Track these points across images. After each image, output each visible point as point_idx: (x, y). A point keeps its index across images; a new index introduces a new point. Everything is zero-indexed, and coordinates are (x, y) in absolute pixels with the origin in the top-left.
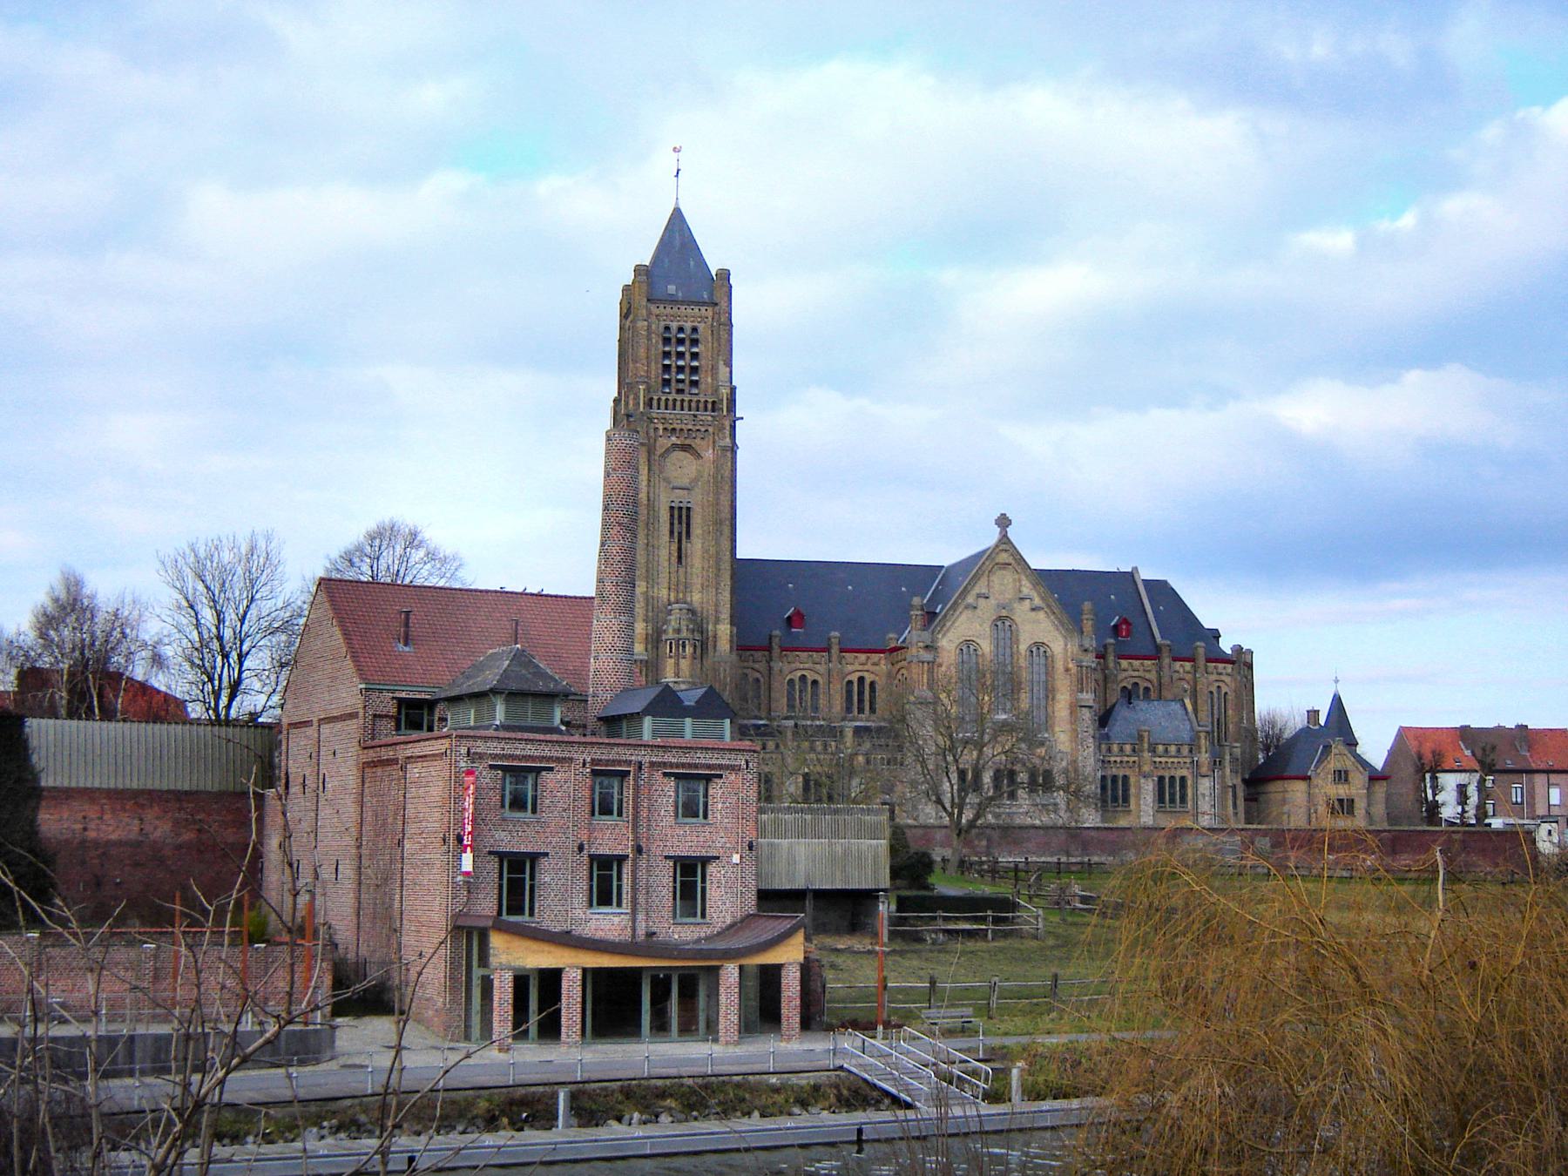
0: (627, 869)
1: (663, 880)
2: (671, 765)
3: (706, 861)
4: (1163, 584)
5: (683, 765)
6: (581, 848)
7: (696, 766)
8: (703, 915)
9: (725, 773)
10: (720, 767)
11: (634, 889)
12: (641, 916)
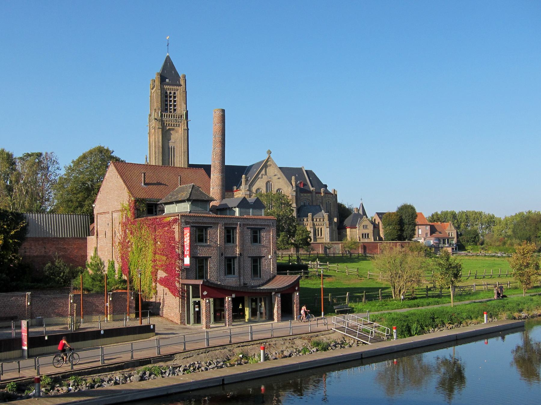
0: (236, 261)
1: (248, 264)
2: (250, 225)
3: (261, 258)
4: (311, 171)
5: (253, 225)
6: (222, 255)
7: (257, 225)
8: (260, 277)
9: (266, 227)
10: (265, 225)
11: (239, 269)
12: (242, 278)
